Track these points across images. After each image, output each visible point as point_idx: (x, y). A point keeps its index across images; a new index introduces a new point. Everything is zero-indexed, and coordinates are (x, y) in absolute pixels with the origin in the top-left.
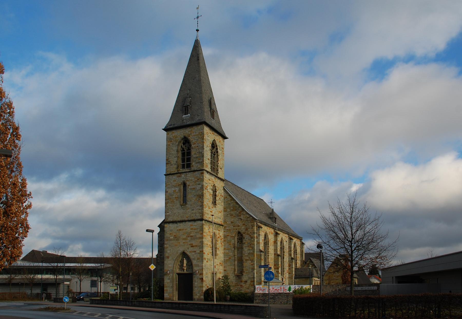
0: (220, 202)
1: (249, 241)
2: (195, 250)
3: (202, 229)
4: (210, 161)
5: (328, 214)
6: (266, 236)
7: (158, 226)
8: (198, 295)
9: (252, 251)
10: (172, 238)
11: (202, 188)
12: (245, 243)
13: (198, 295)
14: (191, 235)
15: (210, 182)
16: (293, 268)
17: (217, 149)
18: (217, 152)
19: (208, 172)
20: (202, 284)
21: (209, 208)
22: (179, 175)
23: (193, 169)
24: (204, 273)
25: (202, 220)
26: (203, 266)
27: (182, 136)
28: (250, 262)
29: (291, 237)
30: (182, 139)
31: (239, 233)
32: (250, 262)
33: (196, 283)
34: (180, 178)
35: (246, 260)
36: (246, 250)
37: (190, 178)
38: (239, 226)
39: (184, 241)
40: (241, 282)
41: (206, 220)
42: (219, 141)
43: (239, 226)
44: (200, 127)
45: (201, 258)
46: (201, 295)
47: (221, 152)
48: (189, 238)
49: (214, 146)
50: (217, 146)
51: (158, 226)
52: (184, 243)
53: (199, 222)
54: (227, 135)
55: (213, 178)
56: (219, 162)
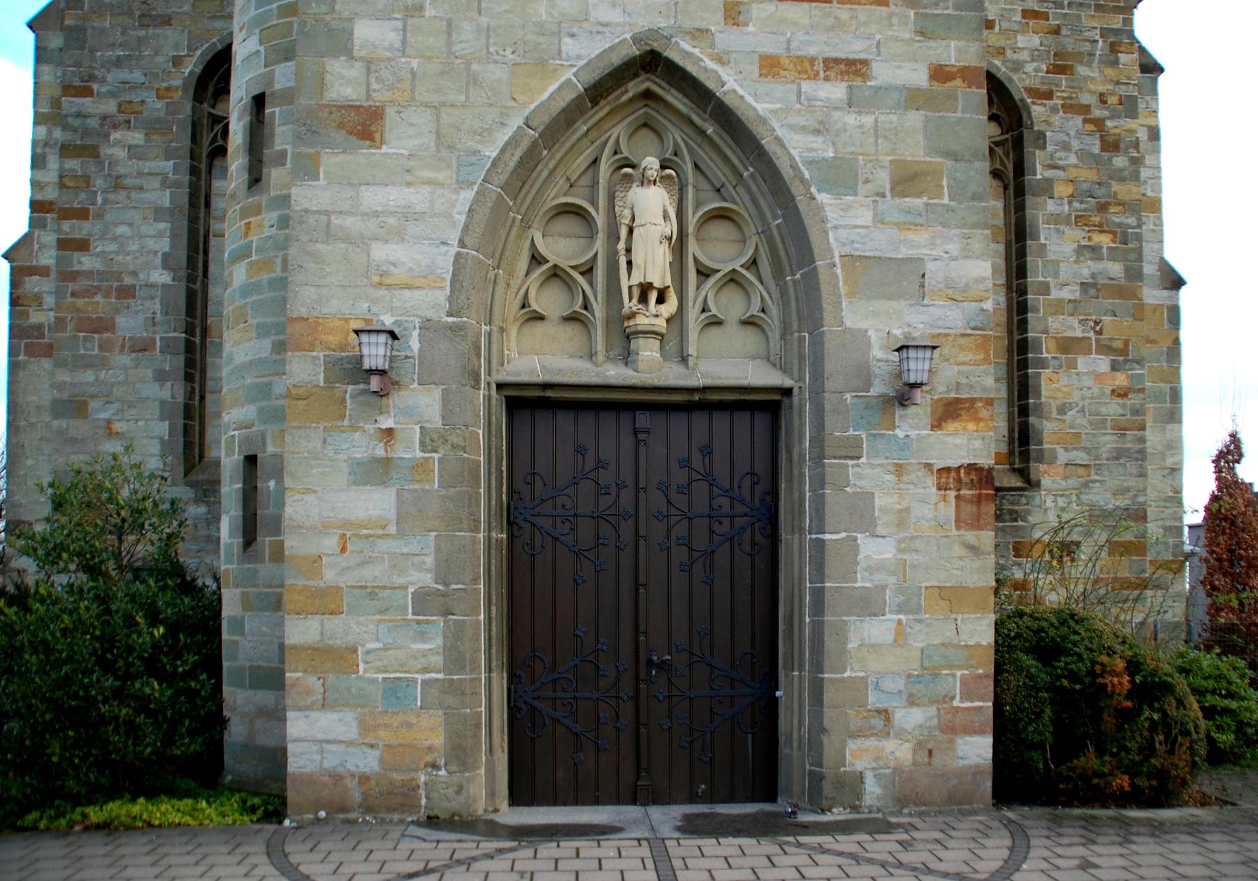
1: (1088, 175)
2: (853, 48)
7: (31, 25)
9: (1115, 269)
12: (1047, 188)
28: (1102, 364)
31: (997, 89)
35: (1068, 346)
36: (1059, 250)
46: (952, 727)
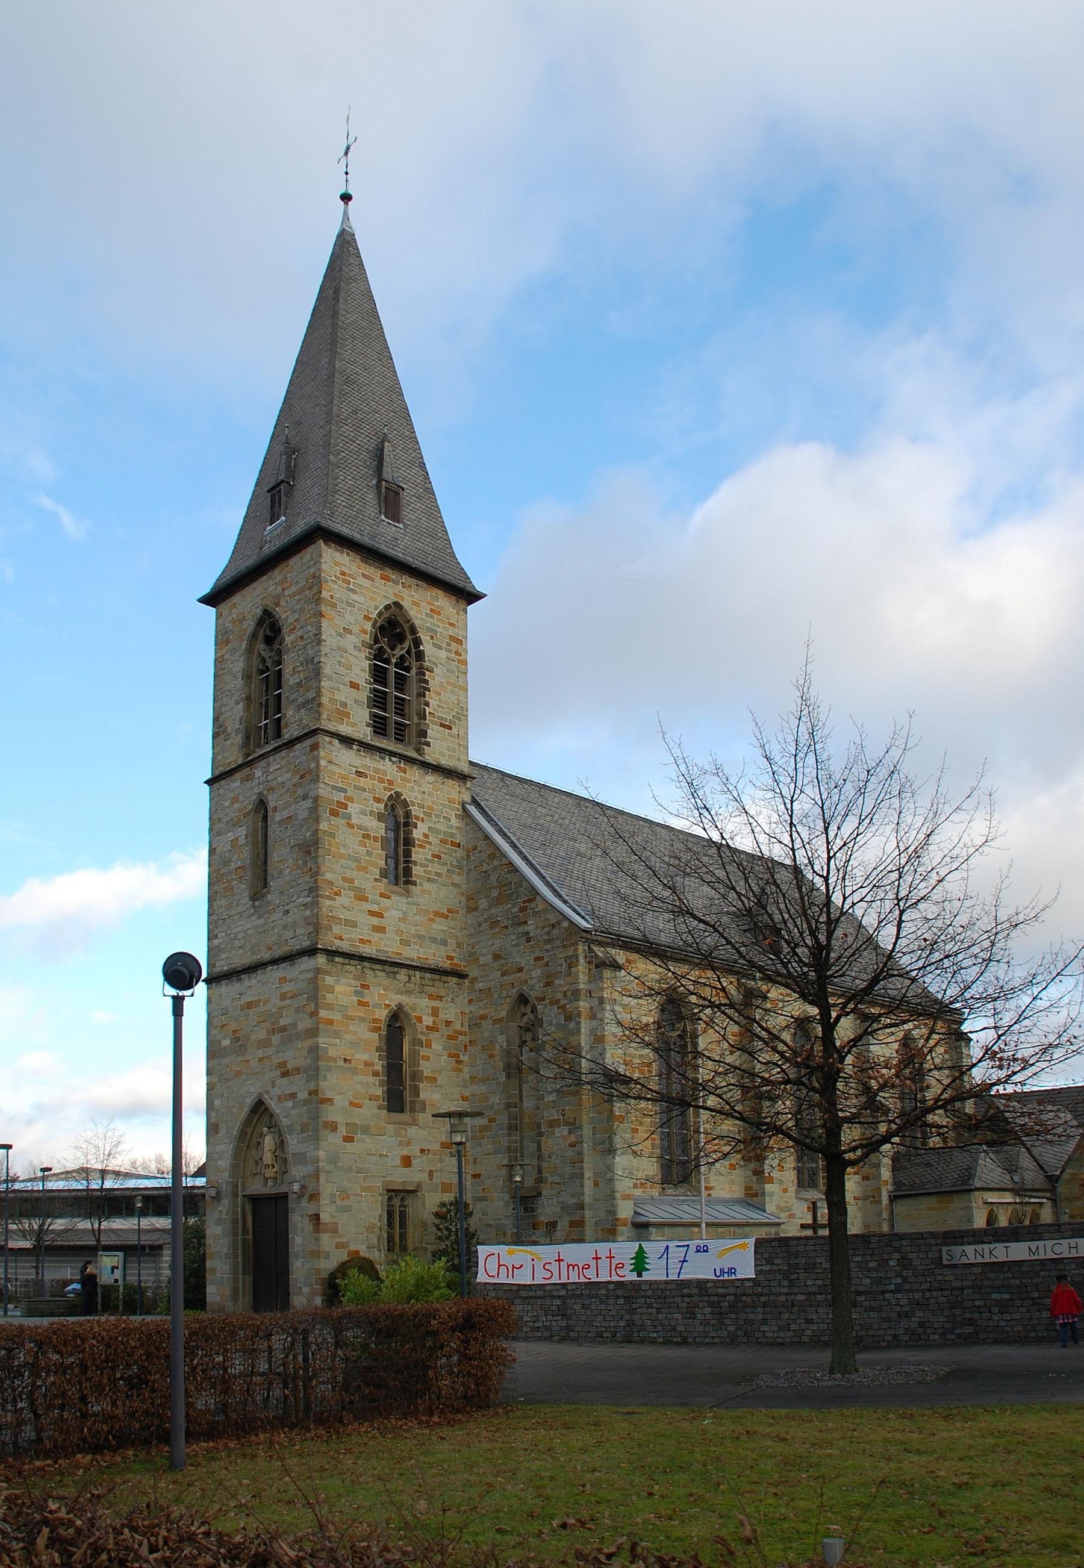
0: (443, 870)
2: (293, 1090)
3: (314, 994)
8: (305, 1295)
10: (226, 1042)
13: (306, 1290)
14: (283, 1022)
17: (417, 642)
18: (420, 656)
21: (361, 898)
22: (246, 771)
23: (287, 735)
25: (311, 951)
27: (259, 612)
28: (565, 1130)
30: (260, 623)
32: (565, 1130)
33: (299, 1238)
34: (248, 785)
35: (552, 1124)
37: (278, 771)
38: (521, 970)
39: (260, 1053)
40: (535, 1226)
41: (332, 953)
42: (425, 608)
43: (521, 970)
44: (307, 554)
46: (313, 1293)
48: (276, 1039)
49: (393, 632)
50: (413, 630)
52: (261, 1060)
53: (305, 964)
55: (388, 767)
56: (431, 698)
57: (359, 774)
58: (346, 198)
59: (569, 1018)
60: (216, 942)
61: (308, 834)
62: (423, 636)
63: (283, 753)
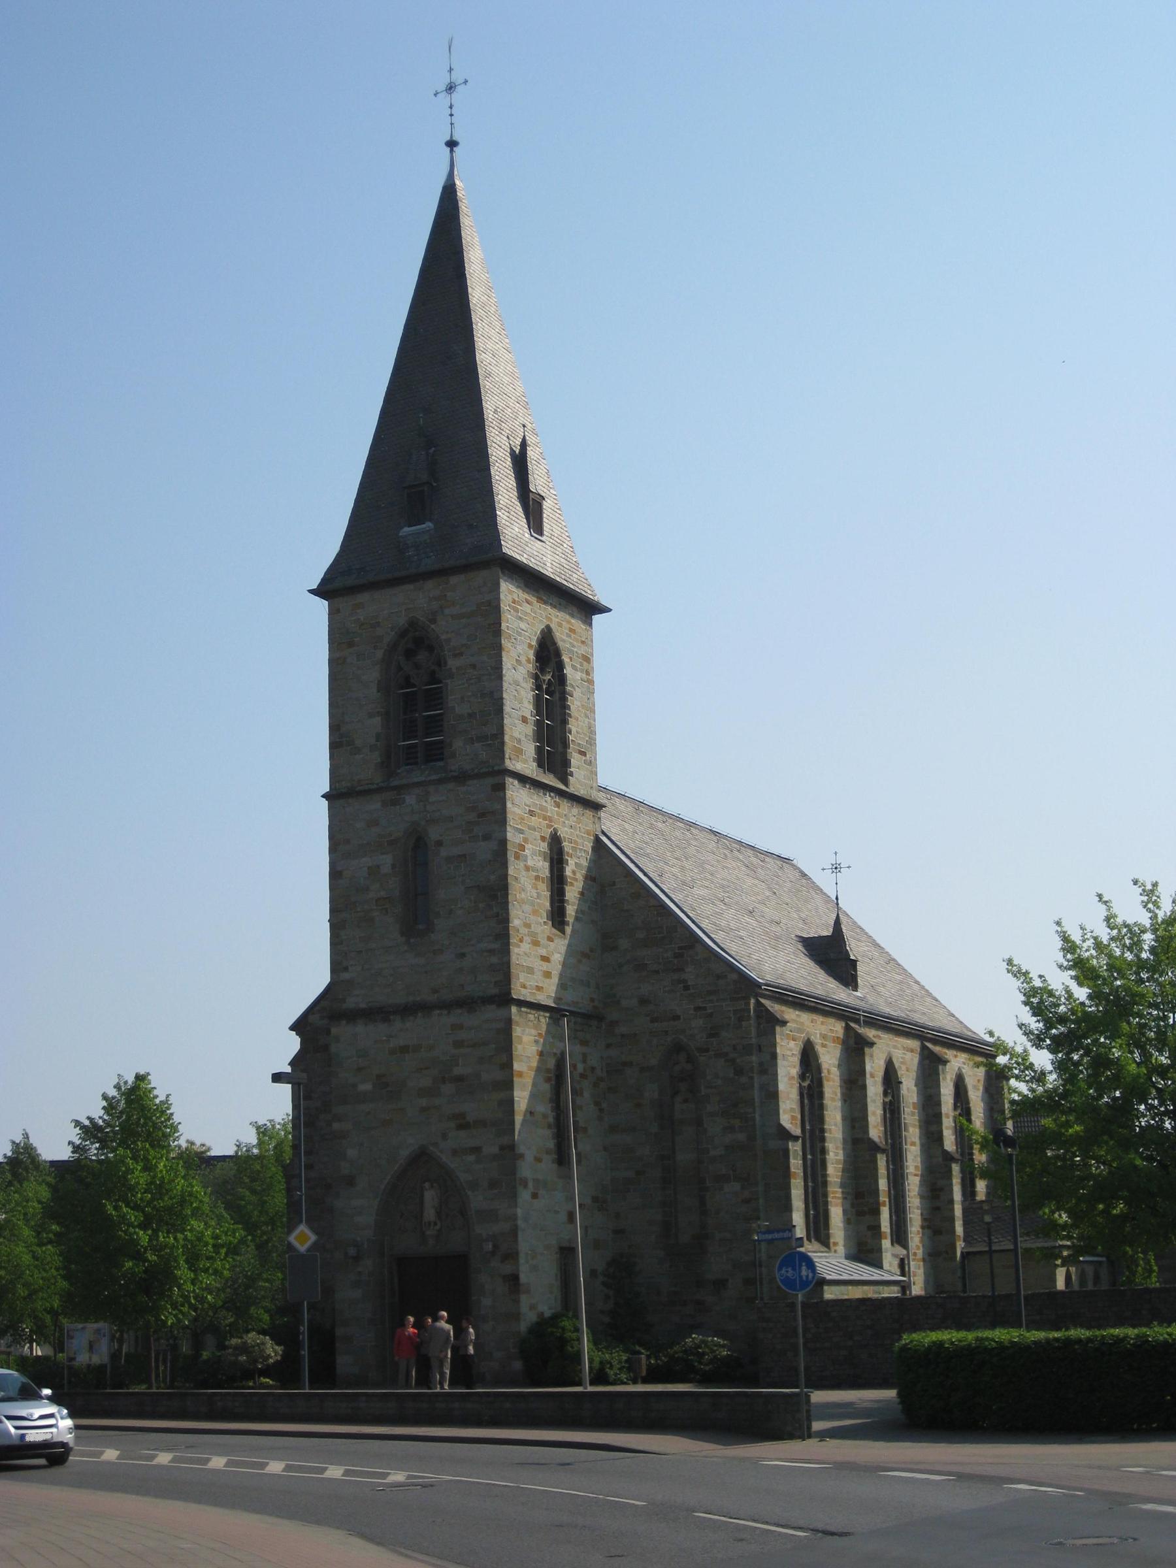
4: (530, 729)
5: (1133, 912)
6: (808, 1057)
7: (292, 1028)
10: (366, 1087)
11: (500, 854)
14: (458, 1071)
15: (535, 821)
16: (951, 1202)
19: (523, 779)
20: (517, 1301)
24: (523, 1246)
26: (514, 1218)
27: (402, 621)
28: (736, 1186)
29: (937, 1049)
30: (403, 634)
39: (424, 1102)
41: (521, 1003)
43: (676, 1018)
45: (506, 1179)
47: (578, 675)
48: (448, 1089)
49: (548, 654)
51: (292, 1028)
52: (423, 1110)
54: (601, 596)
55: (547, 802)
57: (531, 813)
58: (452, 144)
59: (739, 1072)
60: (346, 976)
61: (492, 877)
62: (565, 659)
63: (451, 786)
